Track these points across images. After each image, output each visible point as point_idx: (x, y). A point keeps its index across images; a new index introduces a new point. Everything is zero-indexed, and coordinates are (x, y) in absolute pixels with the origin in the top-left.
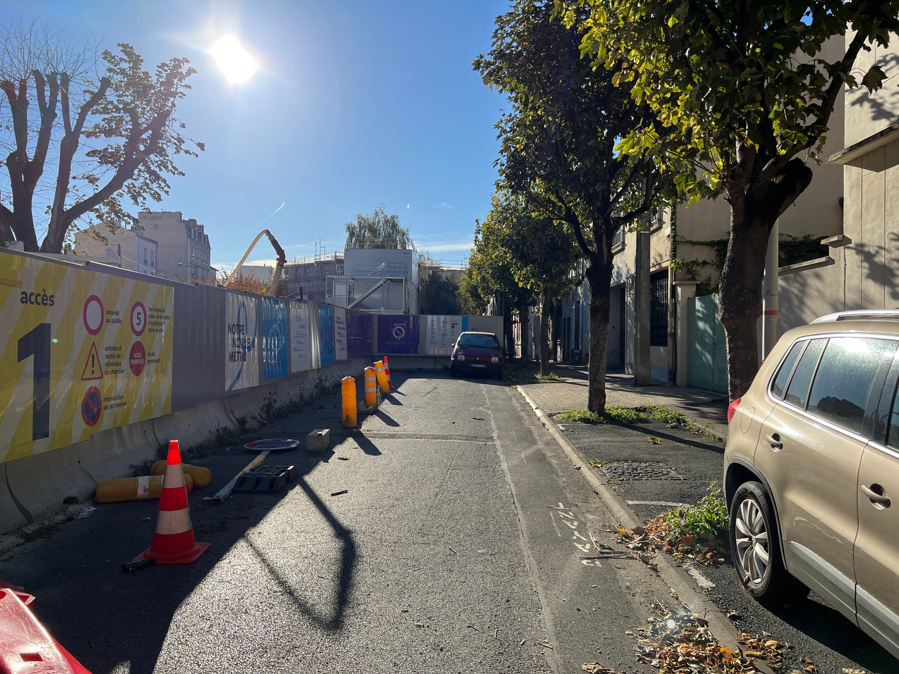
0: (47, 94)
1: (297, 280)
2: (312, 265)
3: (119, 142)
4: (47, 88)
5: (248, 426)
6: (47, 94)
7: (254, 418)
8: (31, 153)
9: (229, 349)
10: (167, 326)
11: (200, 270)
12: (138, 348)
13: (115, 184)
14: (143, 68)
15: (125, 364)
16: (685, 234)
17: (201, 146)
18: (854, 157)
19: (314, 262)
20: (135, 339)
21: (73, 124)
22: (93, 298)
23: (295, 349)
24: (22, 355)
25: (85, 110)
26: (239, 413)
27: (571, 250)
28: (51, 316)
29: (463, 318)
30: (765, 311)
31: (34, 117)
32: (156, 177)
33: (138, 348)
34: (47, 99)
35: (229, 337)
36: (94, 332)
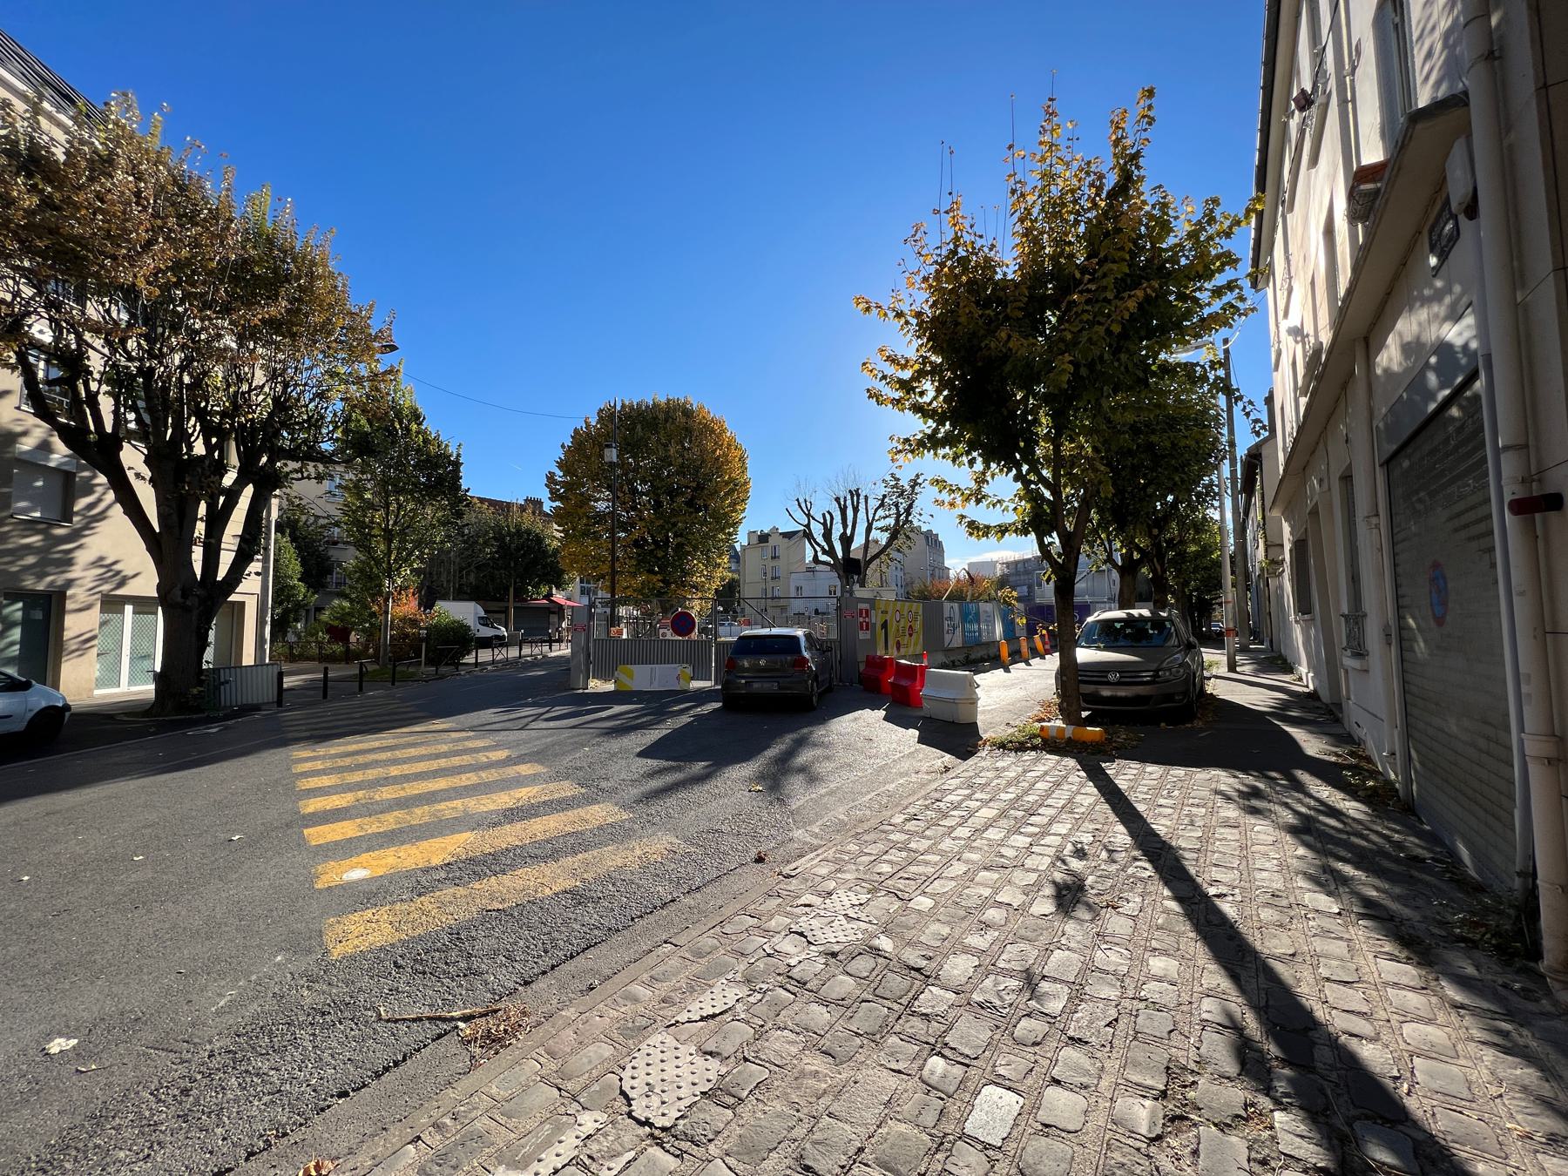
1: (1017, 573)
2: (1030, 559)
3: (891, 521)
4: (855, 498)
8: (849, 532)
9: (946, 627)
13: (889, 544)
14: (901, 483)
16: (1268, 543)
18: (572, 724)
21: (870, 519)
23: (129, 469)
26: (952, 659)
28: (888, 617)
29: (1050, 607)
32: (908, 538)
33: (910, 627)
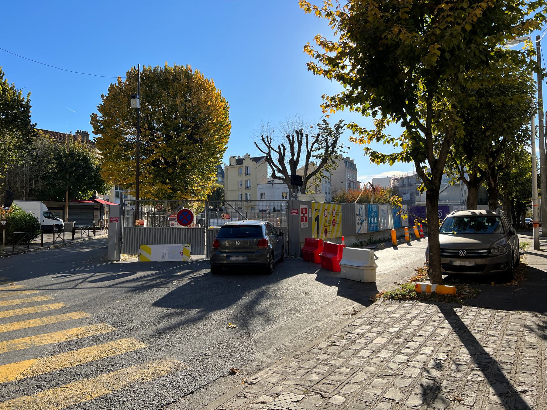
0: (300, 138)
1: (404, 186)
2: (412, 177)
3: (323, 151)
4: (300, 136)
5: (363, 244)
6: (300, 138)
7: (365, 242)
8: (295, 158)
9: (357, 220)
10: (340, 214)
11: (352, 183)
12: (334, 220)
14: (330, 126)
15: (332, 224)
17: (349, 148)
19: (413, 175)
20: (333, 218)
21: (309, 150)
22: (326, 209)
24: (315, 221)
25: (313, 144)
26: (360, 240)
27: (511, 175)
28: (319, 213)
30: (468, 209)
31: (296, 145)
32: (333, 162)
33: (334, 220)
34: (300, 139)
35: (357, 217)
36: (326, 217)
